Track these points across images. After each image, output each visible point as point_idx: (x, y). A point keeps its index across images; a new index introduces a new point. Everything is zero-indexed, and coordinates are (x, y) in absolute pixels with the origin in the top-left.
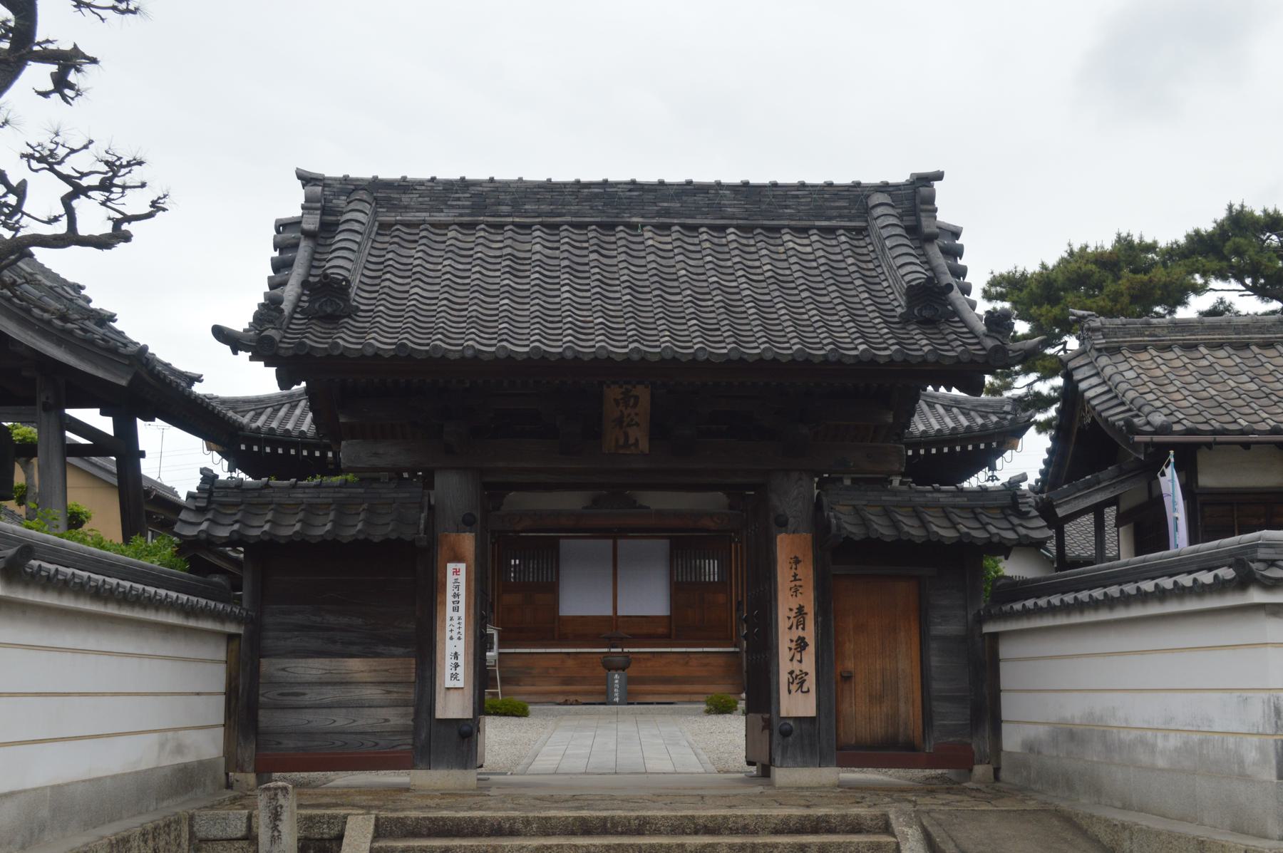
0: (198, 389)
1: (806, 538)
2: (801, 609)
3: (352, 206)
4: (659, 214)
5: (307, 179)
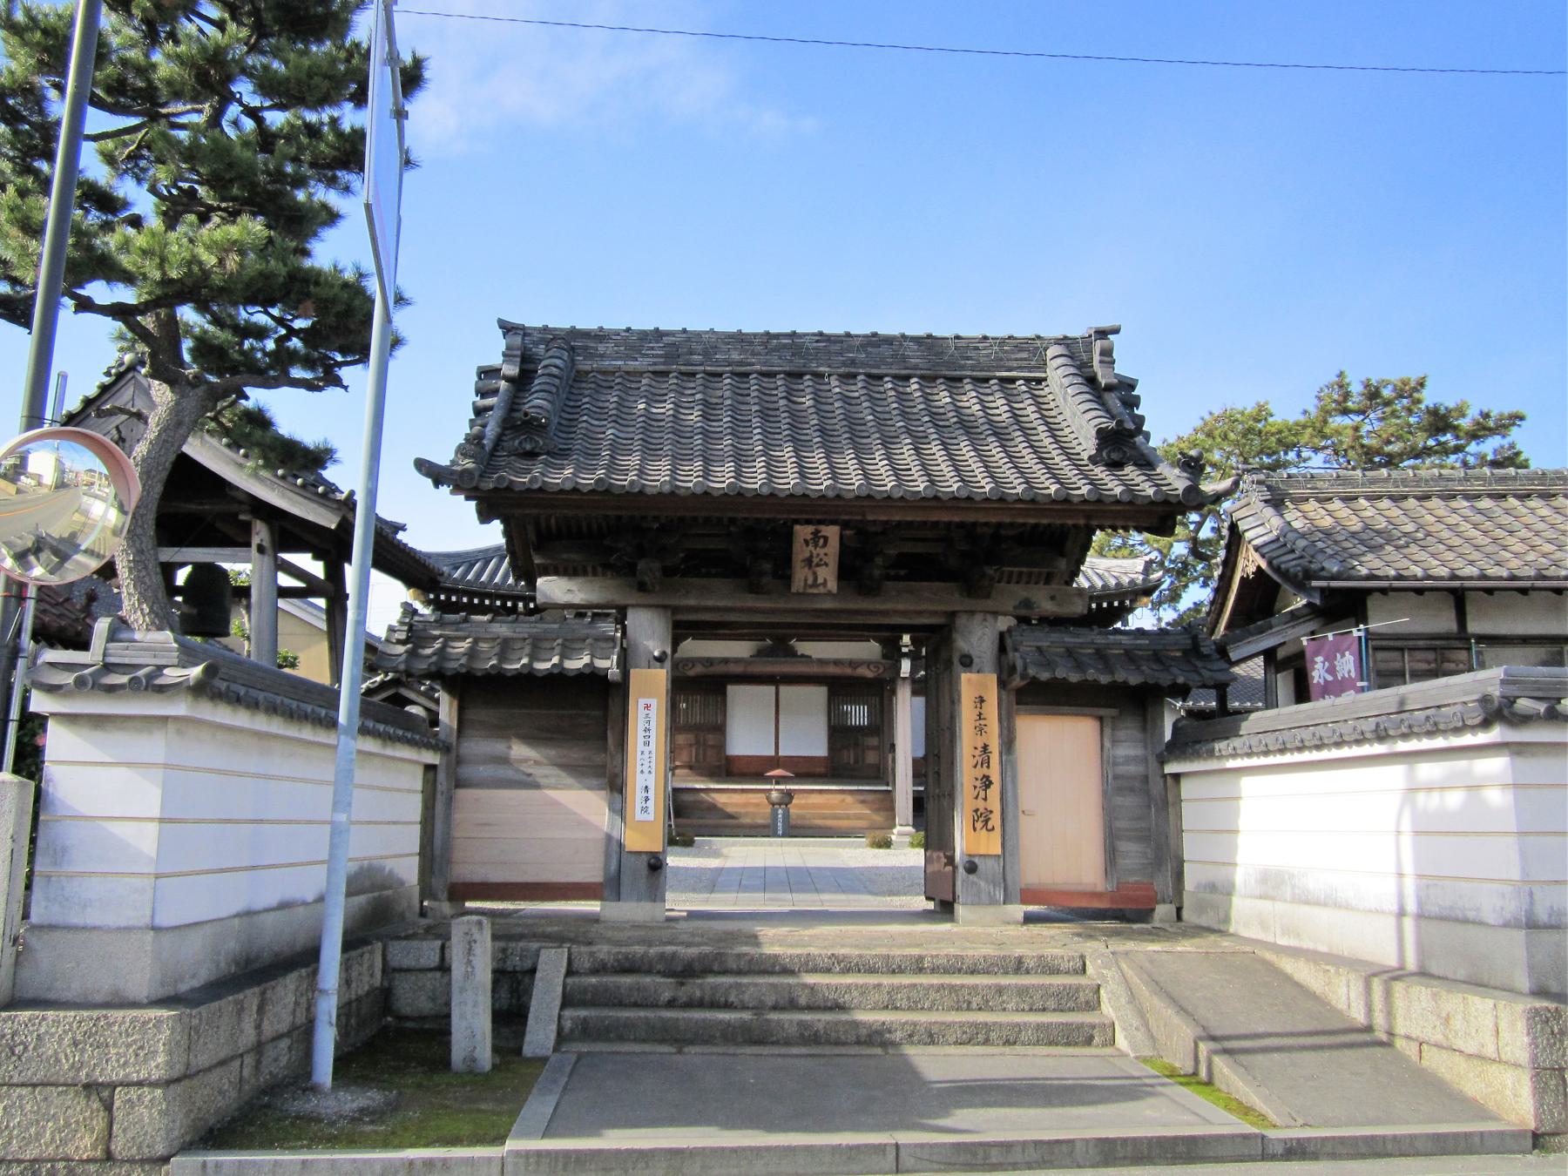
0: (401, 536)
1: (992, 680)
3: (550, 353)
4: (844, 364)
5: (507, 328)
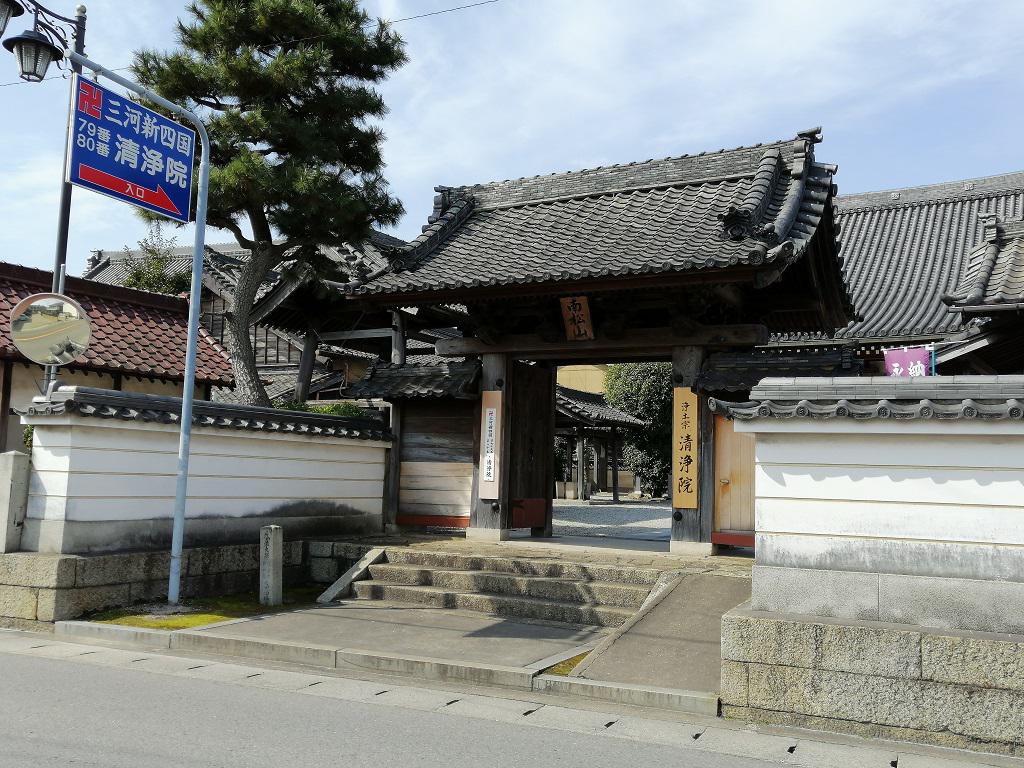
2: (688, 437)
